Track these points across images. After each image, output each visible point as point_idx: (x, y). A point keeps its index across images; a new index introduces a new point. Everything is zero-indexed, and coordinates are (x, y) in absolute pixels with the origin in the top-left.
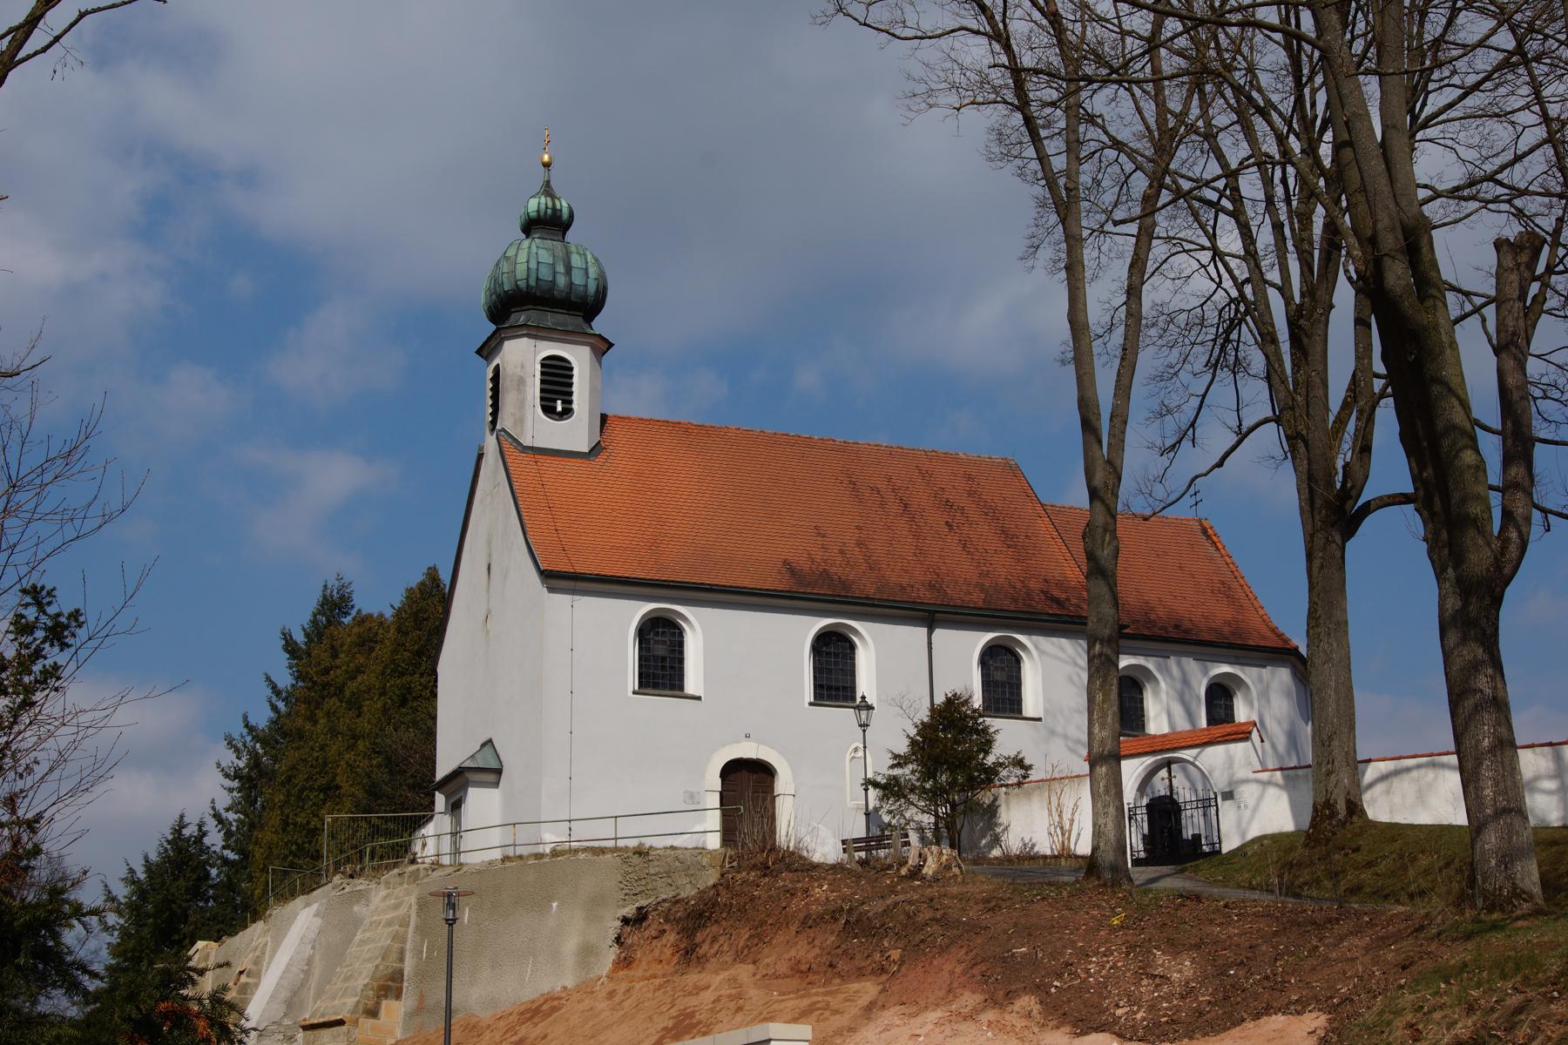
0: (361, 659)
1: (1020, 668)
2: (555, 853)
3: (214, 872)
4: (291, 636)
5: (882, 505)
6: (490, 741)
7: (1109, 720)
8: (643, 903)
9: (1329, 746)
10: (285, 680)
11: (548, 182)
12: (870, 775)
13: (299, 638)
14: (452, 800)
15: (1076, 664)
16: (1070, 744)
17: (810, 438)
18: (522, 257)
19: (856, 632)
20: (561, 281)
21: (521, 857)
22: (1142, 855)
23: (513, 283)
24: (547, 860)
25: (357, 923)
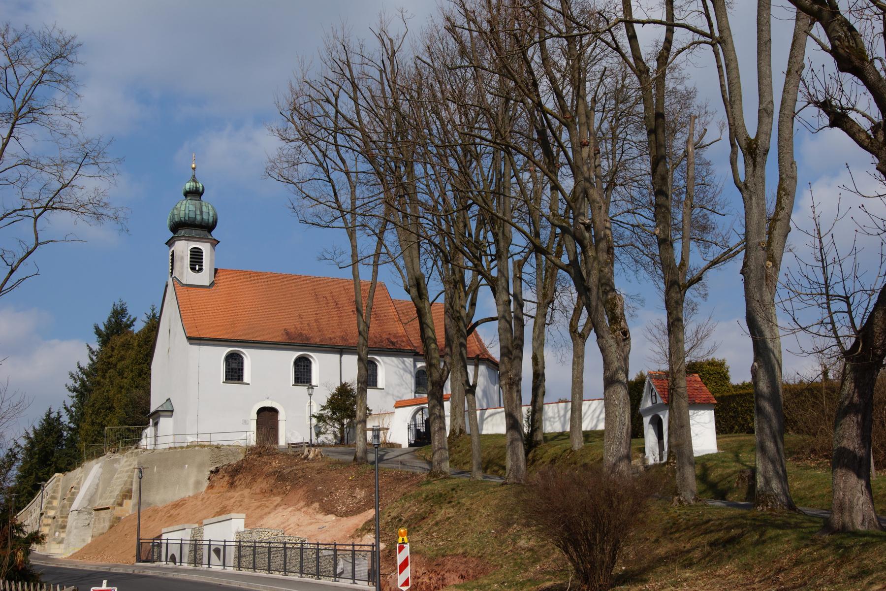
0: (123, 353)
2: (188, 447)
3: (65, 433)
5: (327, 304)
6: (169, 399)
8: (218, 466)
10: (96, 347)
12: (313, 413)
13: (102, 328)
18: (183, 208)
20: (199, 217)
21: (176, 448)
22: (413, 442)
25: (116, 470)
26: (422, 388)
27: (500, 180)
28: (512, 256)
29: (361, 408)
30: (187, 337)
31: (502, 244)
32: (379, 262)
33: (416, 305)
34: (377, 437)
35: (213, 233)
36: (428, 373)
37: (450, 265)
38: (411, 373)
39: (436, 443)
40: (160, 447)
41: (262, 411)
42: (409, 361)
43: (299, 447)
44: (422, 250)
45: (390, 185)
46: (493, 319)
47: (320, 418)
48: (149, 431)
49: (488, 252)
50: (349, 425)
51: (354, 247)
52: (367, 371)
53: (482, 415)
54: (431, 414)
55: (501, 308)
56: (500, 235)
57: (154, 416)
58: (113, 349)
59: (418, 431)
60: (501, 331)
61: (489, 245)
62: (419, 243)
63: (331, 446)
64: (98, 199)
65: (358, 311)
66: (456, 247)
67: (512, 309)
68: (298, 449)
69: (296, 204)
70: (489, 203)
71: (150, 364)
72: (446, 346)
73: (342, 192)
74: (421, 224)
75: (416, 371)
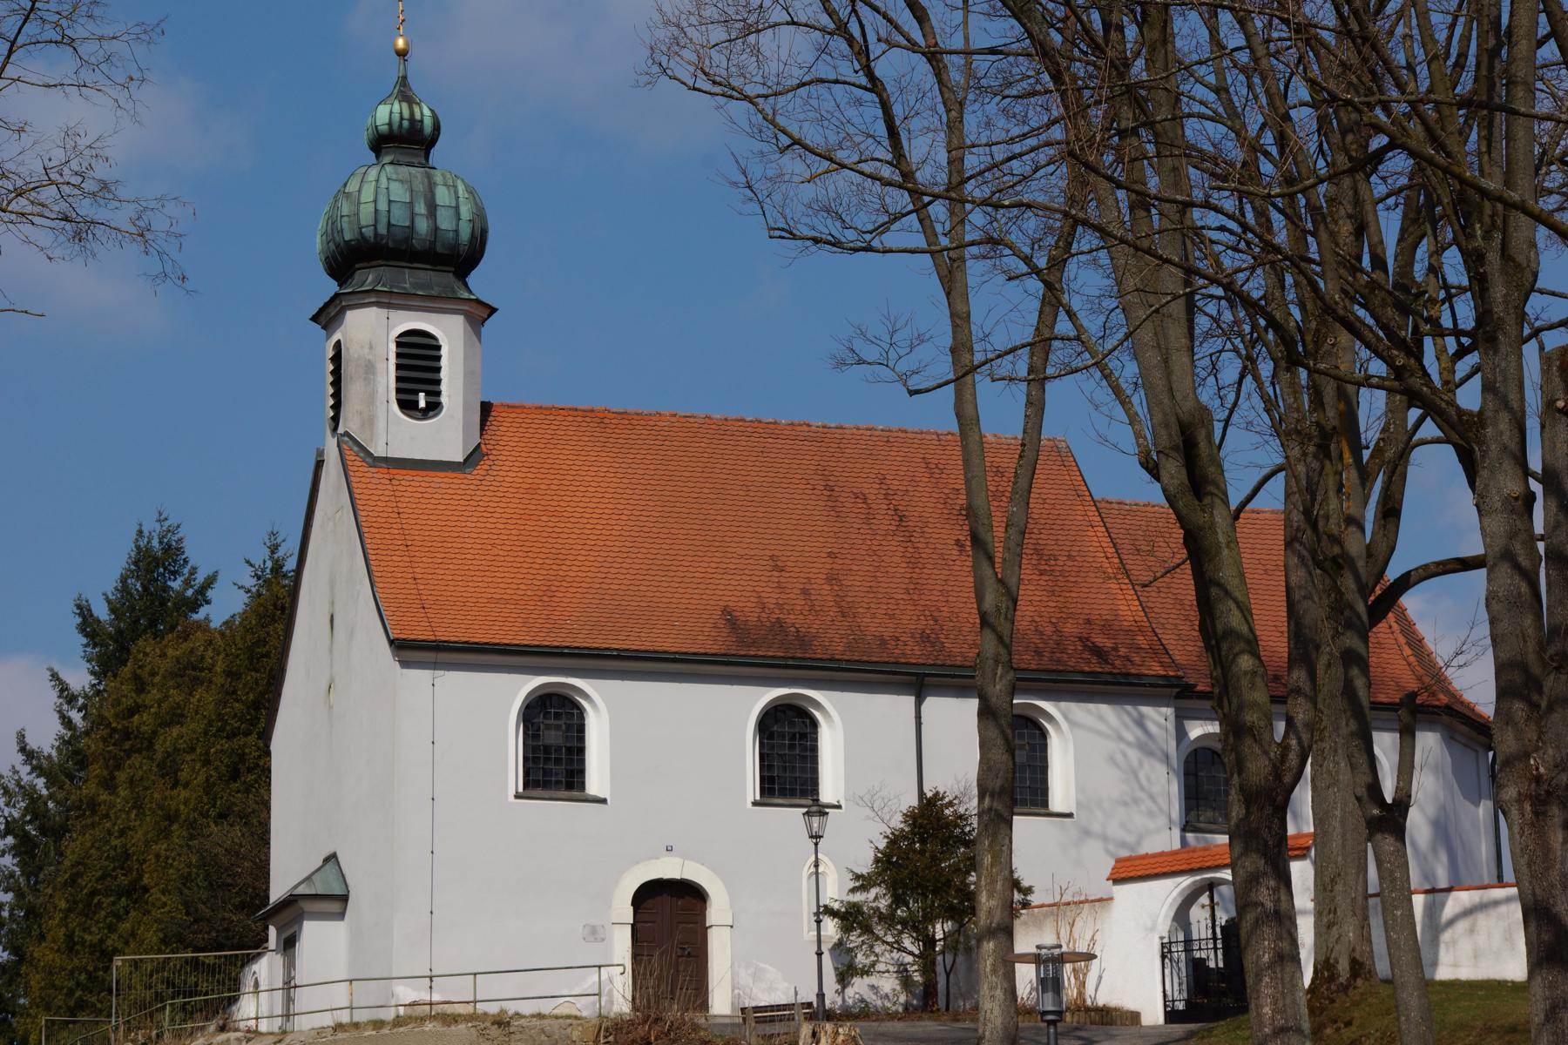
0: (176, 696)
1: (1046, 745)
2: (398, 1022)
4: (90, 610)
7: (999, 886)
9: (1332, 891)
10: (80, 678)
11: (405, 78)
12: (824, 901)
13: (102, 612)
14: (285, 935)
15: (1121, 738)
16: (1111, 847)
17: (775, 423)
18: (367, 195)
19: (817, 705)
20: (422, 226)
21: (356, 1025)
22: (1180, 1006)
23: (356, 230)
24: (386, 1031)
26: (1210, 814)
27: (1494, 54)
28: (1536, 333)
29: (993, 882)
30: (392, 642)
31: (1498, 291)
32: (1050, 371)
33: (1180, 518)
34: (1050, 983)
35: (473, 279)
36: (1229, 759)
37: (1303, 374)
38: (1166, 758)
39: (1267, 1010)
40: (303, 1024)
41: (650, 895)
42: (1159, 717)
43: (781, 1019)
44: (1202, 322)
45: (1087, 93)
46: (1465, 564)
47: (850, 917)
48: (266, 969)
49: (1447, 322)
50: (952, 942)
51: (960, 320)
52: (1011, 751)
53: (1432, 911)
54: (1243, 903)
55: (1498, 524)
56: (1493, 257)
57: (284, 916)
58: (141, 686)
59: (1197, 966)
60: (1496, 606)
61: (1449, 298)
62: (1189, 299)
63: (892, 1016)
64: (74, 165)
65: (977, 541)
66: (1328, 309)
67: (1539, 527)
68: (777, 1028)
69: (756, 171)
70: (1452, 143)
71: (266, 735)
72: (1292, 662)
73: (916, 124)
74: (1197, 231)
75: (1186, 751)
